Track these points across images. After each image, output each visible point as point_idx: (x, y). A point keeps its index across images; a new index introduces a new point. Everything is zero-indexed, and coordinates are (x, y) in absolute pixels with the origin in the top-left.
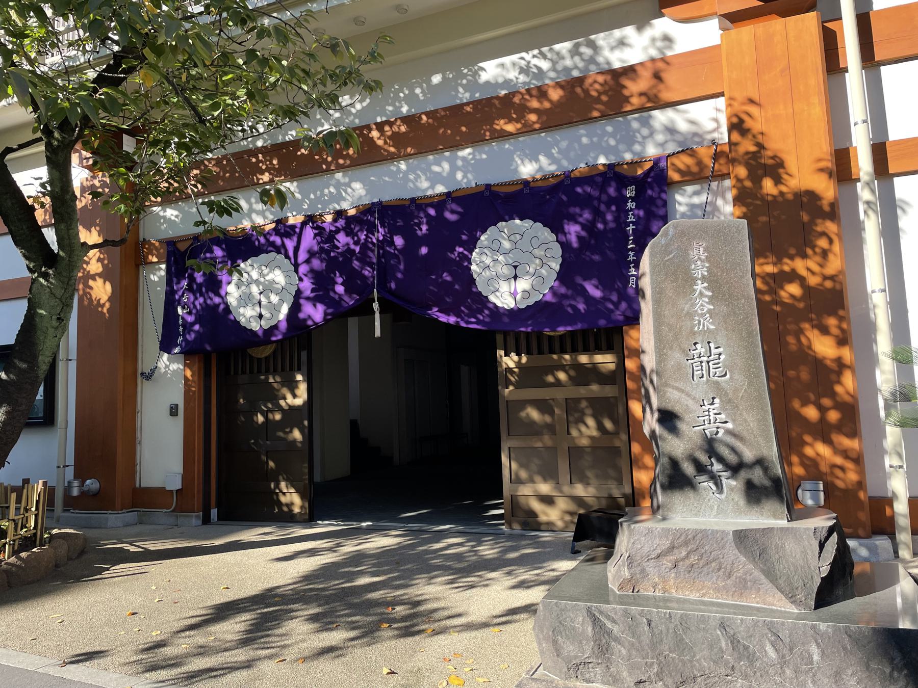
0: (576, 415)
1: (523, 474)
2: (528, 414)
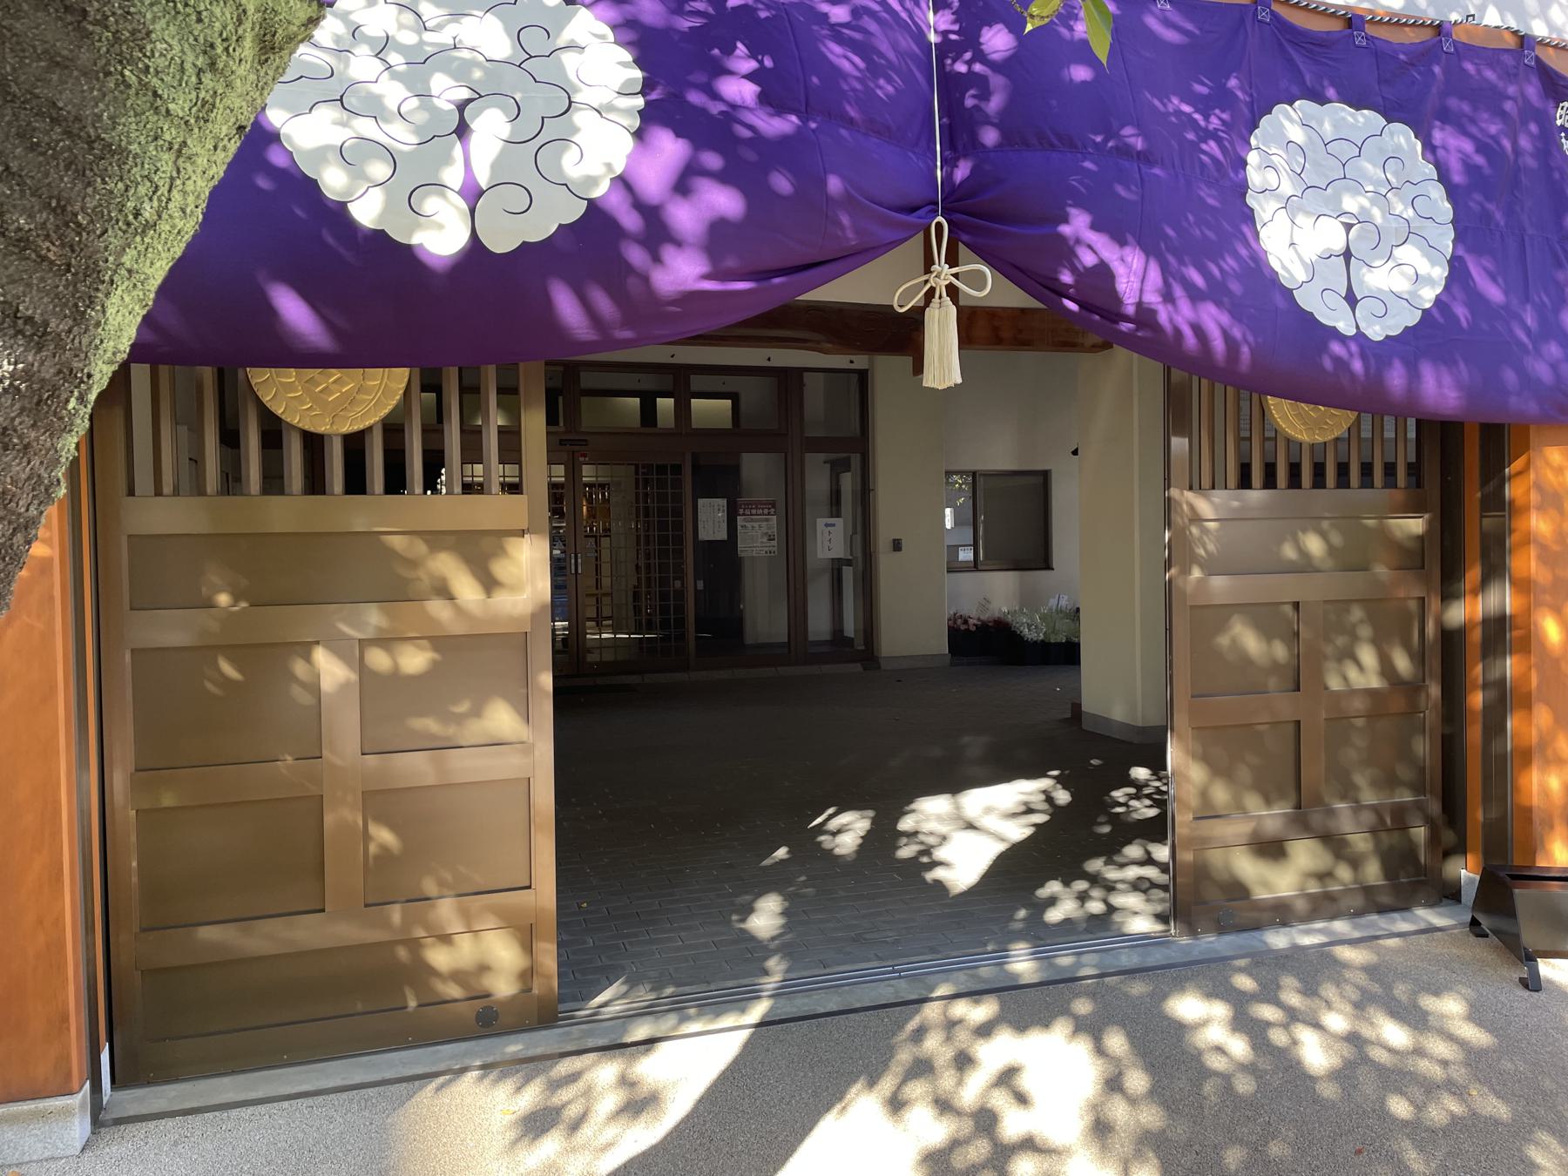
0: (1341, 641)
1: (1221, 794)
2: (1234, 641)
